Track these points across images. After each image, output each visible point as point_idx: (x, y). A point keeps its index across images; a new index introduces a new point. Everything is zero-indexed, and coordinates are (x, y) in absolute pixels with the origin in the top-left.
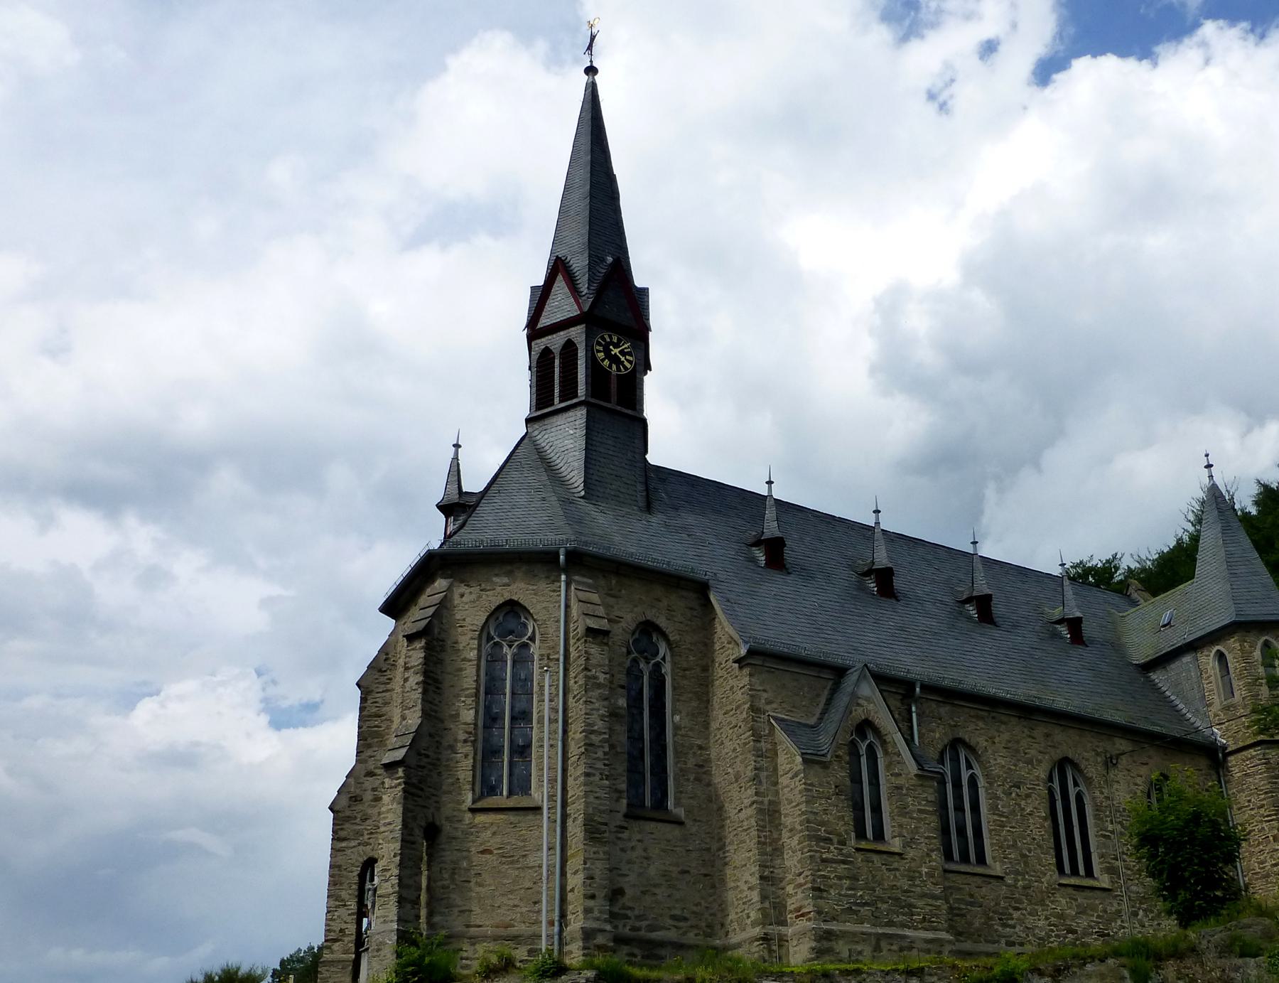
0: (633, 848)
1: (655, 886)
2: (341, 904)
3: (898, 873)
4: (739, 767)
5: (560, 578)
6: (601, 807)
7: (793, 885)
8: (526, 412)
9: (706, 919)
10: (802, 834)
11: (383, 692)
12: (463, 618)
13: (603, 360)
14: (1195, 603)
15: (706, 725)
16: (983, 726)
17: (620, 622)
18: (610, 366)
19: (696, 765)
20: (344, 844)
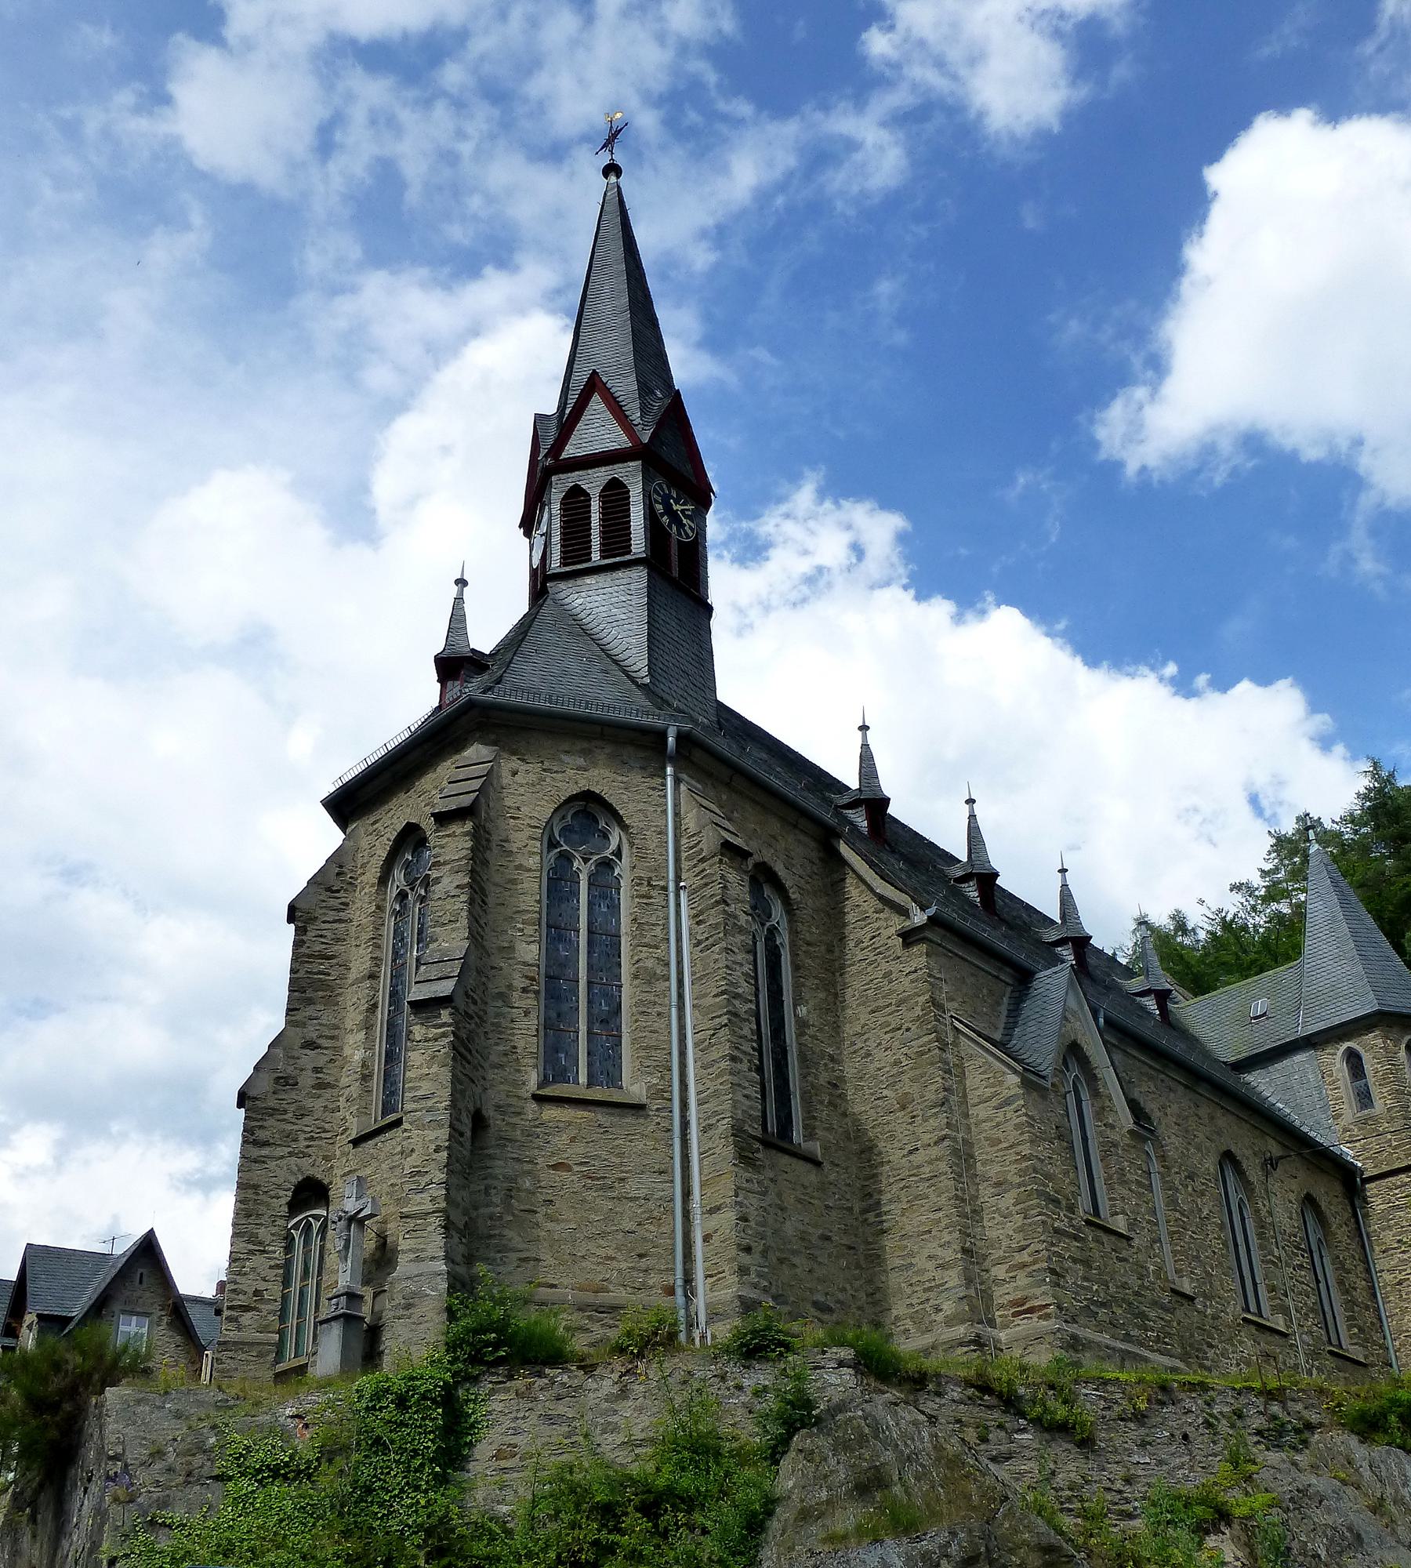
1: (794, 1252)
2: (258, 1248)
4: (907, 1086)
5: (665, 772)
7: (1007, 1266)
9: (854, 1314)
10: (1023, 1189)
11: (335, 921)
12: (517, 805)
13: (662, 515)
14: (1308, 989)
15: (837, 1028)
18: (670, 526)
19: (829, 1083)
20: (265, 1151)
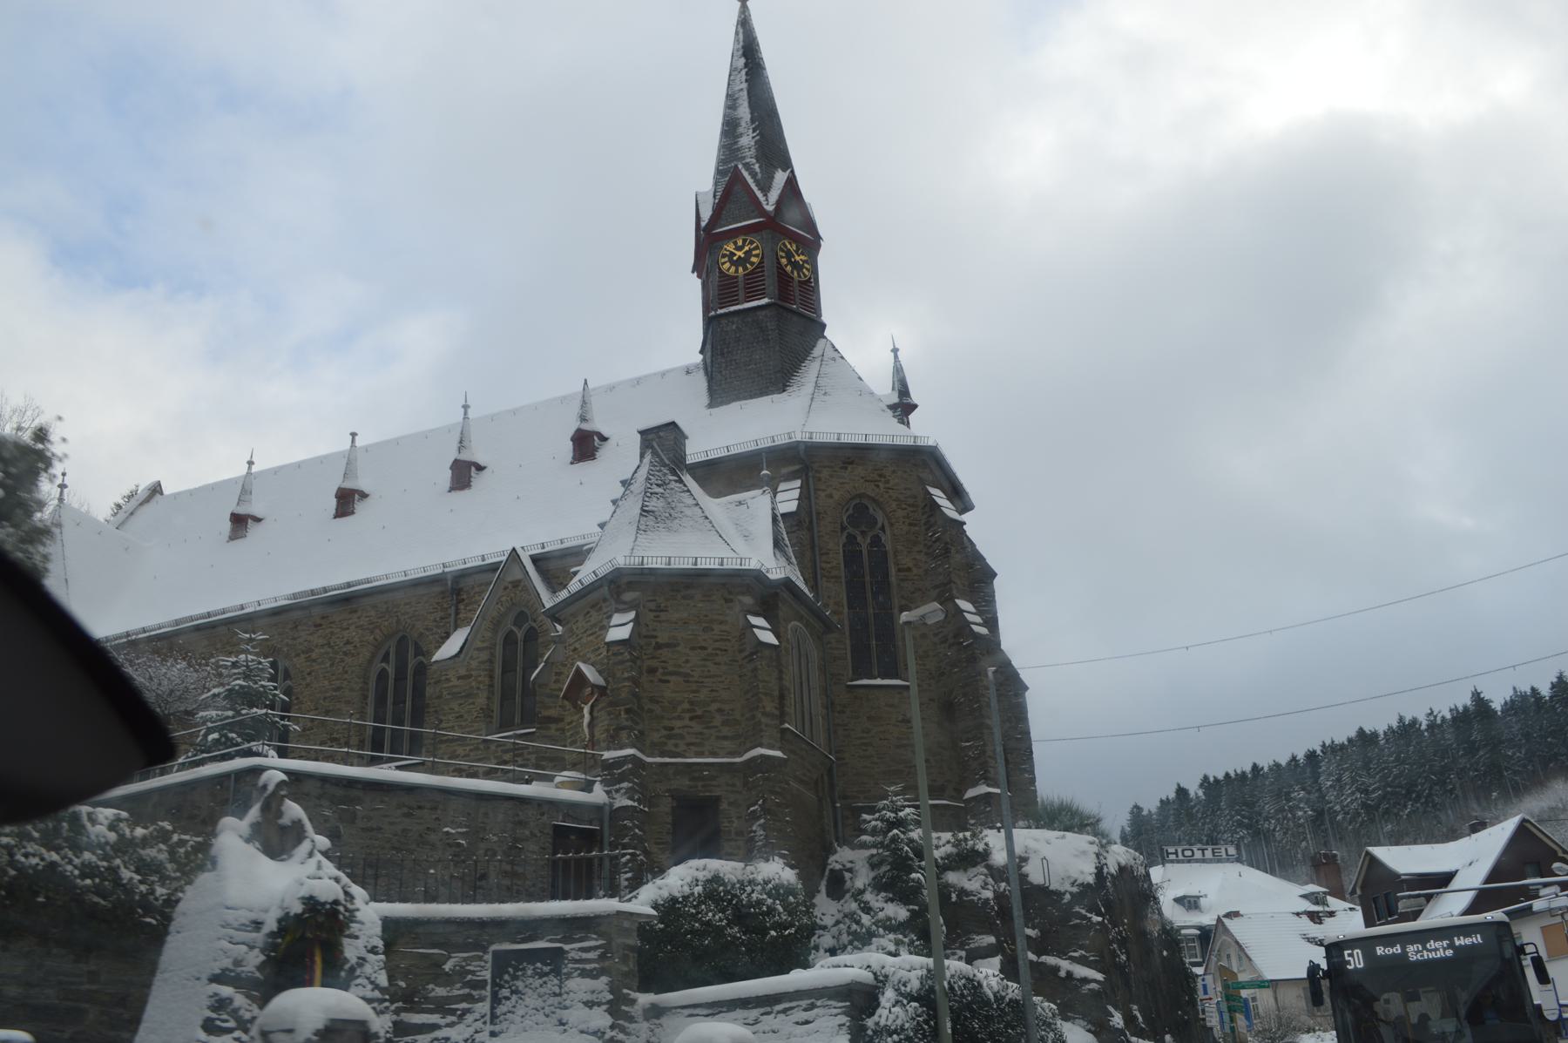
18: (737, 271)
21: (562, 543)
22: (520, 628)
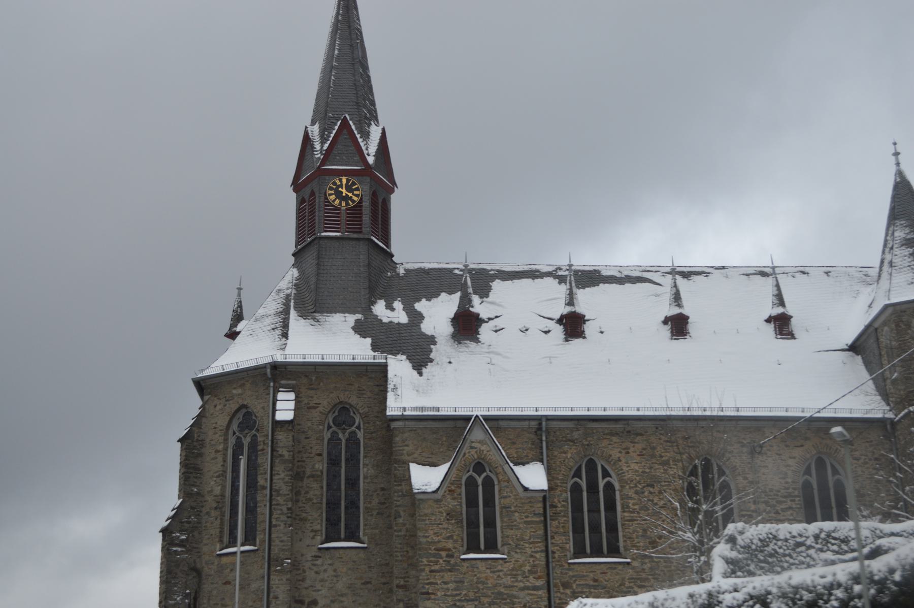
0: (325, 571)
3: (501, 574)
6: (284, 548)
8: (293, 249)
16: (618, 441)
17: (318, 407)
18: (340, 204)
21: (537, 411)
22: (479, 476)
